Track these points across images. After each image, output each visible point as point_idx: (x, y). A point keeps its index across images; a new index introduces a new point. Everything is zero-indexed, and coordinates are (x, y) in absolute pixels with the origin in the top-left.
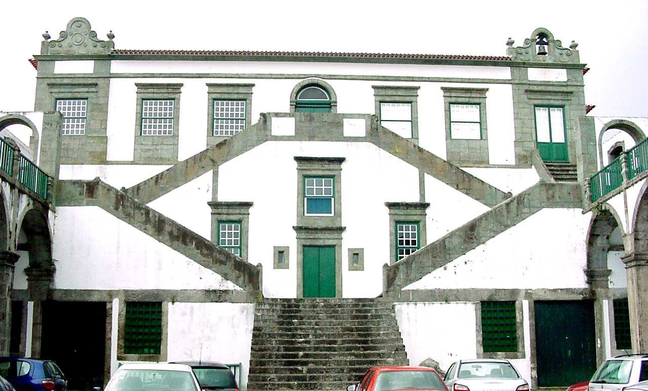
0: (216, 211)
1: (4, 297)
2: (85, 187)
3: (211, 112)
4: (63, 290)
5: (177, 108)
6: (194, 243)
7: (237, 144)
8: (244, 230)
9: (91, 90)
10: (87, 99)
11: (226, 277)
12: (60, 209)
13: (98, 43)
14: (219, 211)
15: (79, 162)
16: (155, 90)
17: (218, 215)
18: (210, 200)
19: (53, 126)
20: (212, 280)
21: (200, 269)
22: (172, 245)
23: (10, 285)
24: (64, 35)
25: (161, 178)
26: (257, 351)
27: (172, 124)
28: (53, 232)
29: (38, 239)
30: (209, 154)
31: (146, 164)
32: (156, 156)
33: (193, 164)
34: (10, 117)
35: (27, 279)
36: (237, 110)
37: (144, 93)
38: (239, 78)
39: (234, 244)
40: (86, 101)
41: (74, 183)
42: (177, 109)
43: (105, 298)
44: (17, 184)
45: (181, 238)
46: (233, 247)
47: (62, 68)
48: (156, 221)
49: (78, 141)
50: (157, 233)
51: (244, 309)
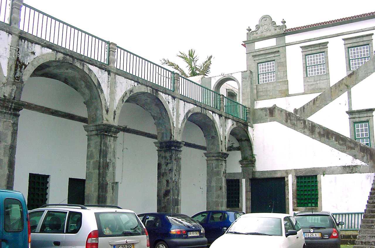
0: (351, 116)
1: (220, 177)
2: (268, 111)
3: (347, 56)
4: (260, 171)
5: (326, 57)
6: (334, 138)
7: (361, 73)
8: (370, 127)
9: (276, 55)
10: (274, 60)
11: (355, 157)
12: (255, 125)
13: (277, 28)
14: (354, 116)
15: (273, 97)
16: (313, 49)
17: (354, 119)
18: (348, 110)
19: (247, 79)
20: (347, 160)
21: (338, 153)
22: (321, 140)
23: (224, 171)
24: (258, 27)
25: (317, 100)
26: (371, 203)
27: (325, 67)
28: (252, 139)
29: (245, 143)
30: (344, 81)
31: (311, 93)
32: (317, 88)
33: (335, 89)
34: (224, 78)
35: (241, 167)
36: (364, 51)
37: (306, 51)
38: (363, 31)
39: (361, 136)
40: (324, 53)
41: (262, 109)
42: (327, 57)
43: (284, 175)
44: (223, 114)
45: (326, 135)
46: (365, 138)
47: (259, 45)
48: (310, 127)
49: (272, 85)
50: (311, 134)
51: (369, 177)
